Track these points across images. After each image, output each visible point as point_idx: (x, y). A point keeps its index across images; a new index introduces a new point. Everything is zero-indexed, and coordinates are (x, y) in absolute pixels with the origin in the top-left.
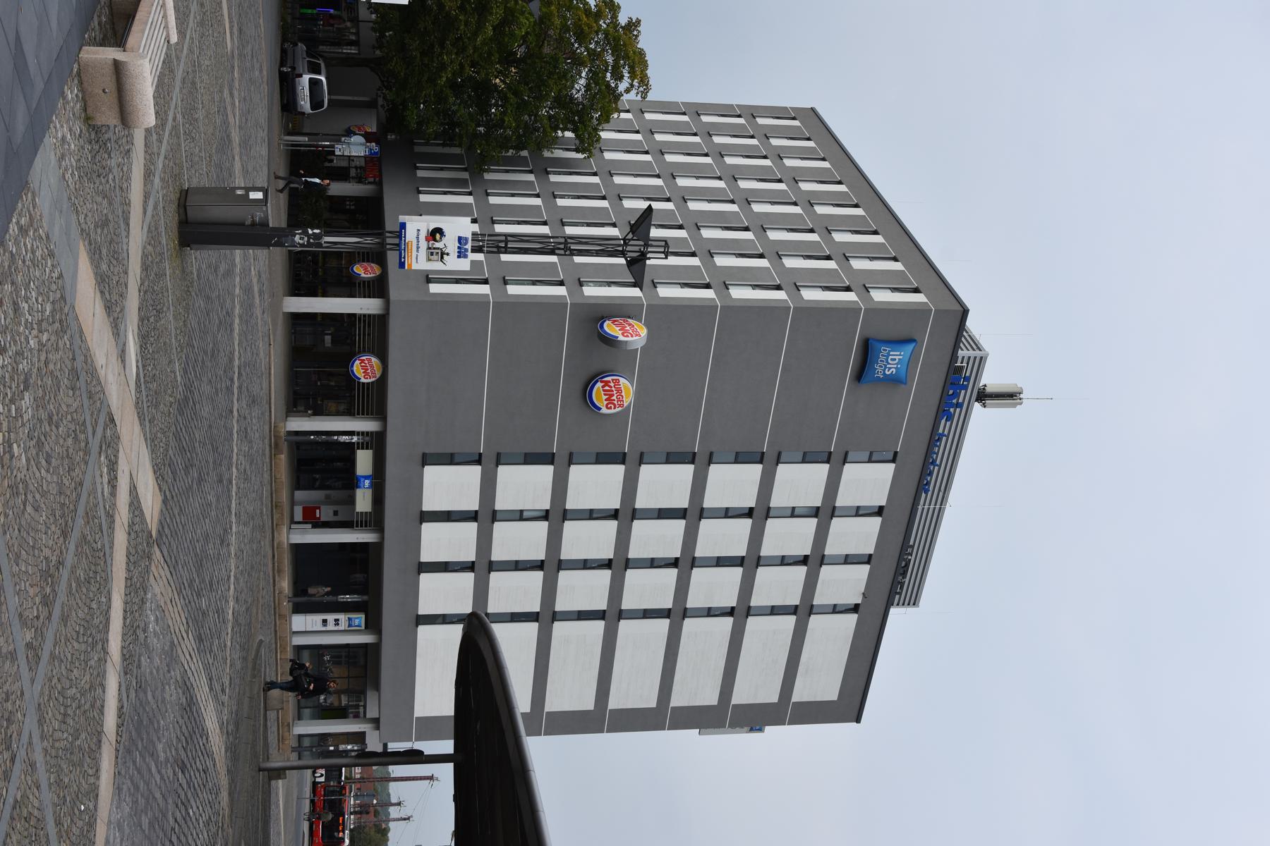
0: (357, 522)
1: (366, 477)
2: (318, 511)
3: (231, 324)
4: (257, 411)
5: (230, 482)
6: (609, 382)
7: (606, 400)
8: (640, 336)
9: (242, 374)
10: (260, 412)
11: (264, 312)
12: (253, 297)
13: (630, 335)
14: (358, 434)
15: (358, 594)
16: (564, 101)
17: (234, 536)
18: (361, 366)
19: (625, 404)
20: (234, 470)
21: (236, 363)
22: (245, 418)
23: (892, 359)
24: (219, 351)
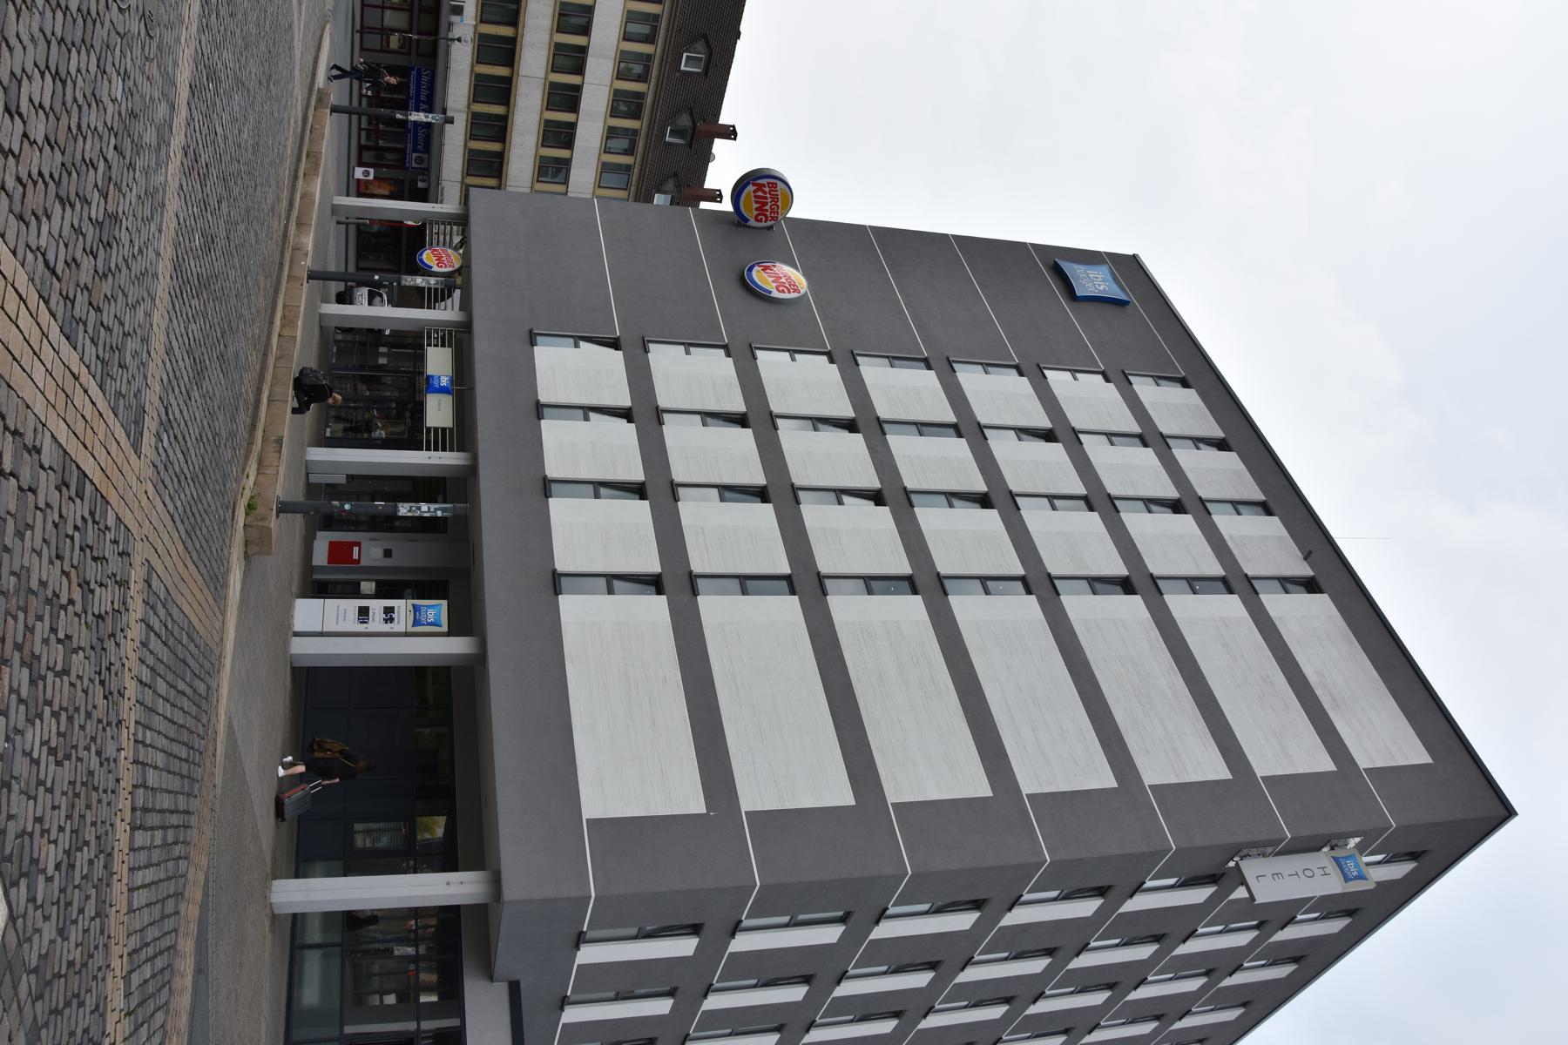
2: (356, 549)
6: (764, 186)
7: (756, 209)
8: (799, 292)
13: (786, 290)
18: (756, 197)
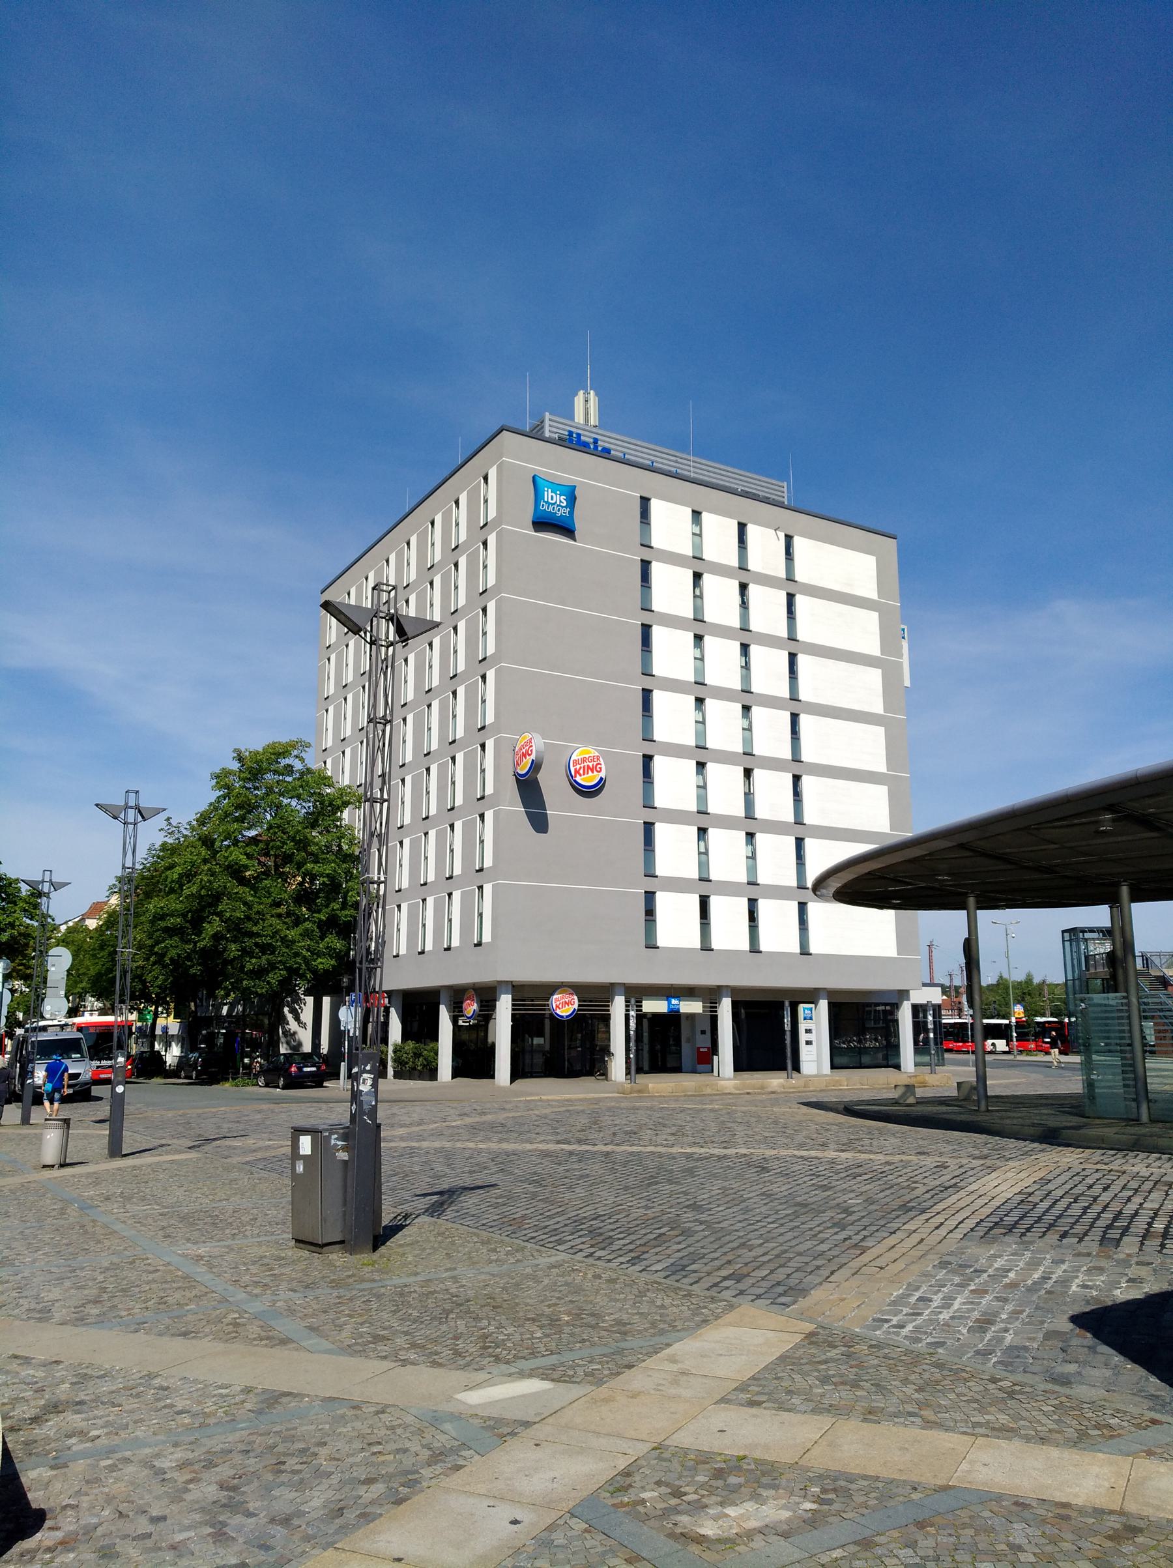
0: (711, 1011)
1: (669, 1003)
2: (701, 1050)
3: (508, 1154)
4: (606, 1118)
5: (689, 1156)
9: (566, 1139)
10: (607, 1113)
11: (504, 1109)
12: (484, 1123)
14: (627, 1010)
15: (637, 1028)
16: (313, 821)
17: (752, 1151)
19: (597, 754)
20: (674, 1150)
21: (551, 1147)
22: (614, 1134)
23: (552, 499)
24: (535, 1173)
